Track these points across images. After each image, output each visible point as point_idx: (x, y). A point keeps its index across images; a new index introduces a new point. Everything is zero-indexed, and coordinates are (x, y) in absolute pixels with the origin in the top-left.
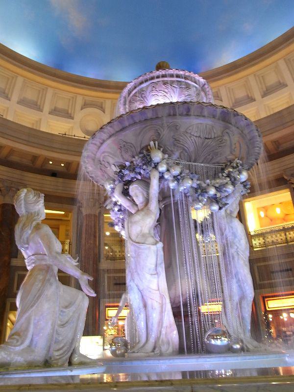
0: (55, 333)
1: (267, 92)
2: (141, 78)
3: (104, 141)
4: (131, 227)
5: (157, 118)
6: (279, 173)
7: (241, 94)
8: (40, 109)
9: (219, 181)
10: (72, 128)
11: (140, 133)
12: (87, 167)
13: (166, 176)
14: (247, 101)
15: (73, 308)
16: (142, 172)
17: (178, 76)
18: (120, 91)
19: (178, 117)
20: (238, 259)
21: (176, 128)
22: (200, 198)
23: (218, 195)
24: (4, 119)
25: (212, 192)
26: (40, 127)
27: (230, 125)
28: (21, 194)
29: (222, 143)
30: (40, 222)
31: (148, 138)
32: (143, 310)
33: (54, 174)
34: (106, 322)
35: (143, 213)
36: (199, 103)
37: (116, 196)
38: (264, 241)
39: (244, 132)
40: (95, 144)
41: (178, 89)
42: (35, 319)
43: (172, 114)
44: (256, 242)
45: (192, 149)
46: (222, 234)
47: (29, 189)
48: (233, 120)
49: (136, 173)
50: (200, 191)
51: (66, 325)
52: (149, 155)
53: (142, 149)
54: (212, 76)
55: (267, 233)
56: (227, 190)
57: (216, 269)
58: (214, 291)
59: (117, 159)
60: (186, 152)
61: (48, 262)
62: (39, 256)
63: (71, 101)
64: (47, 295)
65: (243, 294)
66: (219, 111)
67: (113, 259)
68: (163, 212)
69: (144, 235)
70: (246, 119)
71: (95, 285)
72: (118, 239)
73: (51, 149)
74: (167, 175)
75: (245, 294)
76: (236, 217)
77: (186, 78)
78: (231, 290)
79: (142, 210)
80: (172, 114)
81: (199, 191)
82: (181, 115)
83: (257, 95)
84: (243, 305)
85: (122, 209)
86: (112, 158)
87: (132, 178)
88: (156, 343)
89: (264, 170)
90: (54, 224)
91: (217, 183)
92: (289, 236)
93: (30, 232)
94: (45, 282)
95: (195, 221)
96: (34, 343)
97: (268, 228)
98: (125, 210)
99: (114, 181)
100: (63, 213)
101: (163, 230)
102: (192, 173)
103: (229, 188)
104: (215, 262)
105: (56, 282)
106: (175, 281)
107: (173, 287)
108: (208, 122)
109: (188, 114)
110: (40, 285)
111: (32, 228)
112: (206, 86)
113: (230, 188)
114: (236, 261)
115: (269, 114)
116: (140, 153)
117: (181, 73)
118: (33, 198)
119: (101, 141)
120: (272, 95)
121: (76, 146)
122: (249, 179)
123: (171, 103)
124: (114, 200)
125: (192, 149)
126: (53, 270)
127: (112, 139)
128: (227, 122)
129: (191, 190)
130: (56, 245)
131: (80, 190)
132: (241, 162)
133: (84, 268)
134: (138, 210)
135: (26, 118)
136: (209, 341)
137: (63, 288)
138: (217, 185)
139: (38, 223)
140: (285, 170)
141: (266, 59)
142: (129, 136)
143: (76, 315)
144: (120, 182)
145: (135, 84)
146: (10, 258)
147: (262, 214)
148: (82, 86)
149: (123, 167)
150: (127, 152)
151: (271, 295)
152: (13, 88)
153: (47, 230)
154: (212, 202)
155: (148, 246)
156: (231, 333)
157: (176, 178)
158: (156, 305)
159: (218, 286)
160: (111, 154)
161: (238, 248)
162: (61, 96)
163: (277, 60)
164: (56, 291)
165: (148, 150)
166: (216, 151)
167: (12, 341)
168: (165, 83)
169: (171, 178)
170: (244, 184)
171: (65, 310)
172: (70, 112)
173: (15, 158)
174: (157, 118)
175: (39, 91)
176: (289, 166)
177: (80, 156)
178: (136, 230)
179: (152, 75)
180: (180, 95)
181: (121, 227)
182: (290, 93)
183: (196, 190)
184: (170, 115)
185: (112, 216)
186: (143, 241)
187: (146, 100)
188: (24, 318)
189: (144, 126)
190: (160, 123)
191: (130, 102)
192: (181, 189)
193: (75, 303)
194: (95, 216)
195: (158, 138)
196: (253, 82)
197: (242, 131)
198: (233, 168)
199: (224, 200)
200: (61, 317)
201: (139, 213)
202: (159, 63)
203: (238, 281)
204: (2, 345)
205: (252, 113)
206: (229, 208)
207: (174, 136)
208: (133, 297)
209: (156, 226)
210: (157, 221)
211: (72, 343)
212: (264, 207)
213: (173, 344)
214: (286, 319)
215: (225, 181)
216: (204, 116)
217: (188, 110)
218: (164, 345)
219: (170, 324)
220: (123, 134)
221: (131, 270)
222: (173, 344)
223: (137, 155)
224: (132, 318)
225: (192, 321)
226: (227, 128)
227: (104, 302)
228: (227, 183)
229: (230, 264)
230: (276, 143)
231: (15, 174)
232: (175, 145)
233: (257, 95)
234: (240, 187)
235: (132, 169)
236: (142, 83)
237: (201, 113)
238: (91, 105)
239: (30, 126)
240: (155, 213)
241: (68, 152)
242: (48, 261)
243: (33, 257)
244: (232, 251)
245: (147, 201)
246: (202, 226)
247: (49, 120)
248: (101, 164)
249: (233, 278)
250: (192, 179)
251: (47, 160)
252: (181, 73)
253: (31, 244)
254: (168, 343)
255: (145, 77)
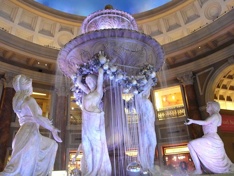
0: (36, 164)
1: (170, 29)
2: (96, 13)
3: (71, 50)
4: (86, 102)
5: (104, 37)
6: (175, 76)
7: (155, 29)
8: (33, 29)
9: (139, 77)
10: (53, 42)
11: (93, 46)
12: (60, 65)
13: (108, 73)
14: (158, 33)
15: (48, 150)
16: (94, 69)
17: (117, 14)
18: (82, 22)
19: (117, 37)
20: (148, 123)
21: (115, 44)
22: (127, 86)
23: (138, 85)
24: (9, 34)
25: (135, 83)
26: (32, 41)
27: (146, 44)
28: (17, 78)
29: (141, 55)
30: (29, 96)
31: (98, 49)
32: (91, 152)
33: (40, 70)
34: (69, 162)
35: (93, 94)
36: (129, 30)
37: (78, 84)
38: (164, 115)
39: (155, 49)
40: (66, 51)
41: (117, 22)
42: (23, 156)
43: (113, 35)
44: (160, 115)
45: (124, 57)
46: (140, 108)
47: (23, 75)
48: (149, 42)
49: (90, 70)
50: (128, 82)
51: (43, 160)
52: (98, 59)
53: (94, 55)
54: (139, 17)
55: (166, 110)
56: (144, 82)
57: (135, 131)
58: (134, 144)
59: (79, 61)
60: (121, 59)
61: (33, 121)
62: (28, 117)
63: (34, 19)
64: (32, 141)
65: (150, 143)
66: (141, 35)
67: (76, 124)
68: (105, 94)
69: (93, 107)
70: (156, 41)
71: (63, 135)
72: (80, 112)
73: (40, 55)
74: (108, 71)
75: (151, 143)
76: (149, 98)
77: (122, 15)
78: (143, 141)
79: (93, 92)
80: (113, 35)
81: (127, 82)
82: (118, 36)
83: (164, 30)
84: (150, 149)
85: (81, 92)
86: (76, 60)
87: (88, 73)
88: (98, 171)
89: (165, 75)
90: (41, 101)
91: (138, 78)
92: (179, 112)
93: (22, 102)
94: (31, 133)
95: (124, 101)
96: (23, 171)
97: (167, 108)
98: (83, 92)
99: (77, 74)
100: (45, 95)
101: (105, 105)
102: (123, 71)
103: (145, 81)
104: (135, 126)
105: (38, 134)
106: (111, 135)
107: (110, 139)
108: (133, 42)
109: (122, 36)
110: (27, 135)
111: (24, 99)
112: (134, 21)
113: (145, 81)
114: (147, 124)
115: (170, 42)
116: (93, 58)
117: (120, 12)
118: (25, 81)
119: (70, 50)
120: (171, 31)
121: (54, 53)
122: (157, 77)
123: (113, 29)
124: (76, 86)
125: (124, 57)
126: (36, 126)
127: (76, 49)
128: (145, 43)
129: (122, 81)
130: (38, 111)
131: (56, 81)
132: (152, 66)
133: (55, 125)
134: (90, 92)
135: (24, 34)
136: (129, 170)
137: (42, 137)
138: (138, 79)
139: (27, 96)
140: (178, 75)
141: (170, 9)
142: (87, 47)
143: (50, 155)
144: (80, 75)
145: (92, 16)
146: (10, 122)
147: (164, 99)
148: (60, 17)
149: (82, 66)
150: (85, 56)
151: (167, 146)
152: (16, 14)
153: (34, 101)
154: (134, 89)
155: (96, 114)
156: (143, 166)
157: (114, 74)
158: (99, 149)
159: (136, 141)
160: (75, 57)
161: (148, 116)
162: (46, 22)
163: (176, 11)
164: (37, 138)
165: (98, 57)
166: (139, 59)
167: (8, 170)
168: (110, 18)
169: (111, 74)
170: (154, 79)
171: (42, 151)
172: (52, 32)
173: (15, 59)
174: (104, 37)
175: (33, 18)
176: (180, 73)
177: (56, 60)
178: (88, 104)
179: (102, 12)
180: (118, 25)
181: (79, 102)
182: (183, 31)
183: (125, 81)
184: (111, 36)
185: (75, 97)
186: (93, 111)
187: (98, 27)
188: (16, 155)
189: (96, 42)
190: (105, 40)
191: (89, 27)
192: (117, 80)
193: (49, 146)
194: (65, 97)
195: (104, 49)
196: (162, 22)
197: (153, 49)
198: (148, 69)
199: (141, 88)
200: (40, 155)
201: (91, 94)
202: (107, 6)
203: (148, 135)
204: (1, 173)
205: (162, 40)
206: (144, 93)
207: (113, 48)
208: (85, 144)
209: (101, 103)
210: (102, 100)
211: (46, 171)
212: (165, 96)
213: (108, 171)
214: (175, 160)
215: (142, 77)
216: (132, 38)
217: (123, 34)
218: (103, 173)
219: (107, 160)
220: (83, 46)
221: (85, 128)
222: (108, 172)
223: (91, 59)
224: (84, 160)
225: (120, 159)
226: (145, 46)
227: (69, 150)
228: (144, 78)
229: (143, 126)
230: (174, 58)
231: (15, 69)
232: (114, 54)
233: (164, 30)
234: (151, 81)
235: (88, 67)
236: (96, 16)
237: (130, 36)
238: (66, 29)
239: (26, 39)
240: (101, 94)
241: (50, 57)
242: (33, 120)
243: (24, 118)
244: (145, 118)
245: (96, 87)
246: (128, 103)
247: (38, 37)
248: (69, 64)
249: (144, 134)
250: (123, 75)
251: (36, 61)
252: (120, 12)
253: (23, 109)
254: (105, 171)
255: (98, 13)
